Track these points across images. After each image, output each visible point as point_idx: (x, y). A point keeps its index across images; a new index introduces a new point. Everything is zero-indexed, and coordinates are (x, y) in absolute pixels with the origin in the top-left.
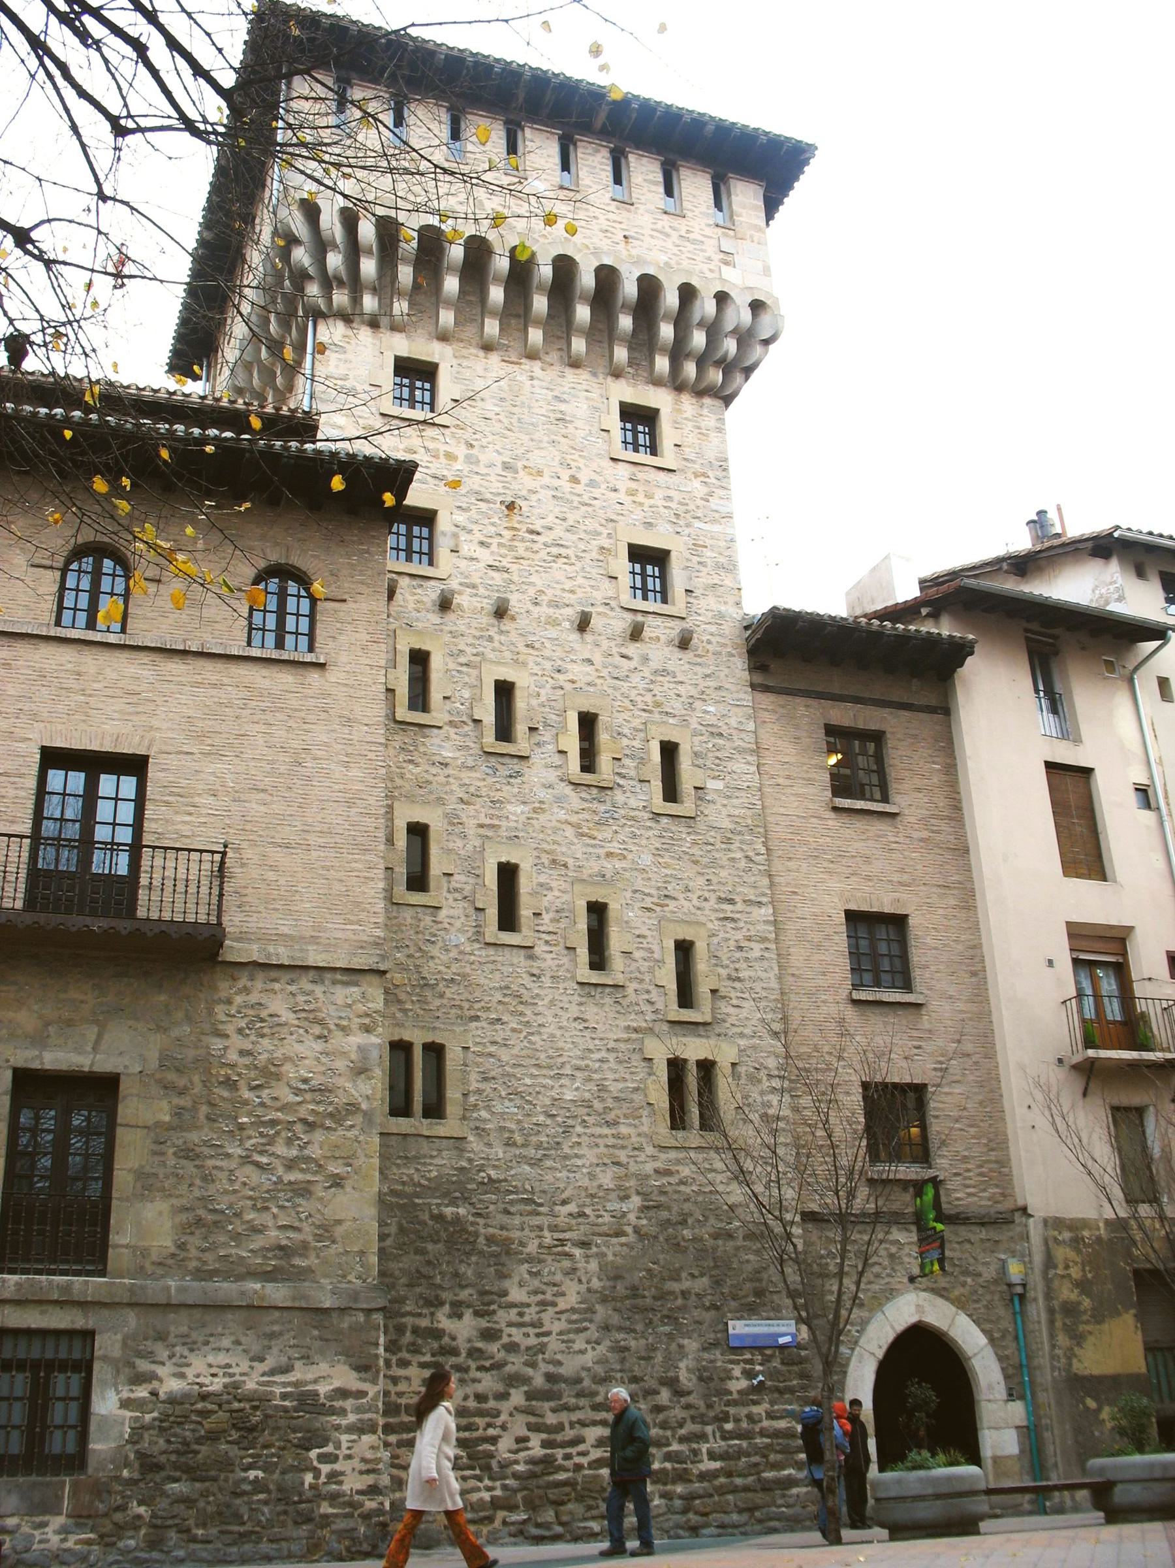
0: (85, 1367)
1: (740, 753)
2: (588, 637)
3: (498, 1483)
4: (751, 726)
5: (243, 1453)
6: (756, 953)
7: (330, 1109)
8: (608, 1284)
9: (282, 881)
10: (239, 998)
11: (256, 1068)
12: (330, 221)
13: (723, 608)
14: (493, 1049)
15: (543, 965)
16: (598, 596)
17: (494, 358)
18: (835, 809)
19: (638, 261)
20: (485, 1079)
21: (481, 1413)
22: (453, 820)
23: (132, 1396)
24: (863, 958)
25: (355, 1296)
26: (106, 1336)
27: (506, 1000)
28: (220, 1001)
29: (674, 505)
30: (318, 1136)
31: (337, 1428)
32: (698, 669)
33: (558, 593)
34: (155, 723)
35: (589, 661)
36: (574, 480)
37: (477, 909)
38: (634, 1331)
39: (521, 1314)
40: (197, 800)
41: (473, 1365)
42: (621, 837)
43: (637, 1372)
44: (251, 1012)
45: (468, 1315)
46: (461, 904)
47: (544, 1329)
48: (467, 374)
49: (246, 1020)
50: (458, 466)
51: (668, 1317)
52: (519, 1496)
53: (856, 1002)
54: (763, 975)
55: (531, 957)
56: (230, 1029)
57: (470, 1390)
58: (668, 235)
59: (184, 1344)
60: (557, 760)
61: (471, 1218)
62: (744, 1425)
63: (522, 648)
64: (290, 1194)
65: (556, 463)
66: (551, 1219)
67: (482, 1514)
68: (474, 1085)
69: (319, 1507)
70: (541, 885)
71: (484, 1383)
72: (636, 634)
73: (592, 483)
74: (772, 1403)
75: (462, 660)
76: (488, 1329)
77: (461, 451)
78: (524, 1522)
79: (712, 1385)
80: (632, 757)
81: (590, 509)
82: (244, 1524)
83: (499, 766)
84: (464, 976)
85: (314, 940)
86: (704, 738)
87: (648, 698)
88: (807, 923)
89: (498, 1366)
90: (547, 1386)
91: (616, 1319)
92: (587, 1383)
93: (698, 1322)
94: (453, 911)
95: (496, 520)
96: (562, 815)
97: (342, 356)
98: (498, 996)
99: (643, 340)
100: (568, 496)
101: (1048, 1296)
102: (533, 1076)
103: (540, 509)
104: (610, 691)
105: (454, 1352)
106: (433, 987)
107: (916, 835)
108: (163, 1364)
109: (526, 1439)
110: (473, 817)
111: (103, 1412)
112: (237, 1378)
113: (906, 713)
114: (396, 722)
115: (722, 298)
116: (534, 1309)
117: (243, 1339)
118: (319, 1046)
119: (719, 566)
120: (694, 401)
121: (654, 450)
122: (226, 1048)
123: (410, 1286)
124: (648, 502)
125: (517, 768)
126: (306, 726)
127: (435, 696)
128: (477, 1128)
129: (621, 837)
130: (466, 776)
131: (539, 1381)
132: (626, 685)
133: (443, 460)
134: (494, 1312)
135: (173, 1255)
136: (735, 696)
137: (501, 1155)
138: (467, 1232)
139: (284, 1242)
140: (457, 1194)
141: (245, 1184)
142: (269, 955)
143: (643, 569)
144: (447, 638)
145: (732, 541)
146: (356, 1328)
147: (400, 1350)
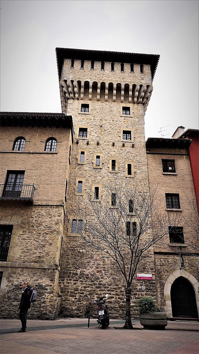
12: (69, 83)
13: (141, 140)
17: (99, 102)
18: (163, 174)
22: (87, 180)
24: (177, 203)
25: (51, 266)
29: (132, 123)
36: (113, 121)
43: (117, 284)
49: (37, 215)
56: (34, 217)
57: (83, 286)
58: (131, 77)
60: (107, 169)
61: (85, 252)
70: (103, 191)
72: (123, 146)
73: (117, 121)
77: (92, 118)
91: (113, 272)
92: (107, 285)
99: (126, 95)
103: (107, 126)
107: (181, 178)
118: (50, 219)
125: (100, 170)
133: (89, 120)
141: (33, 244)
143: (126, 135)
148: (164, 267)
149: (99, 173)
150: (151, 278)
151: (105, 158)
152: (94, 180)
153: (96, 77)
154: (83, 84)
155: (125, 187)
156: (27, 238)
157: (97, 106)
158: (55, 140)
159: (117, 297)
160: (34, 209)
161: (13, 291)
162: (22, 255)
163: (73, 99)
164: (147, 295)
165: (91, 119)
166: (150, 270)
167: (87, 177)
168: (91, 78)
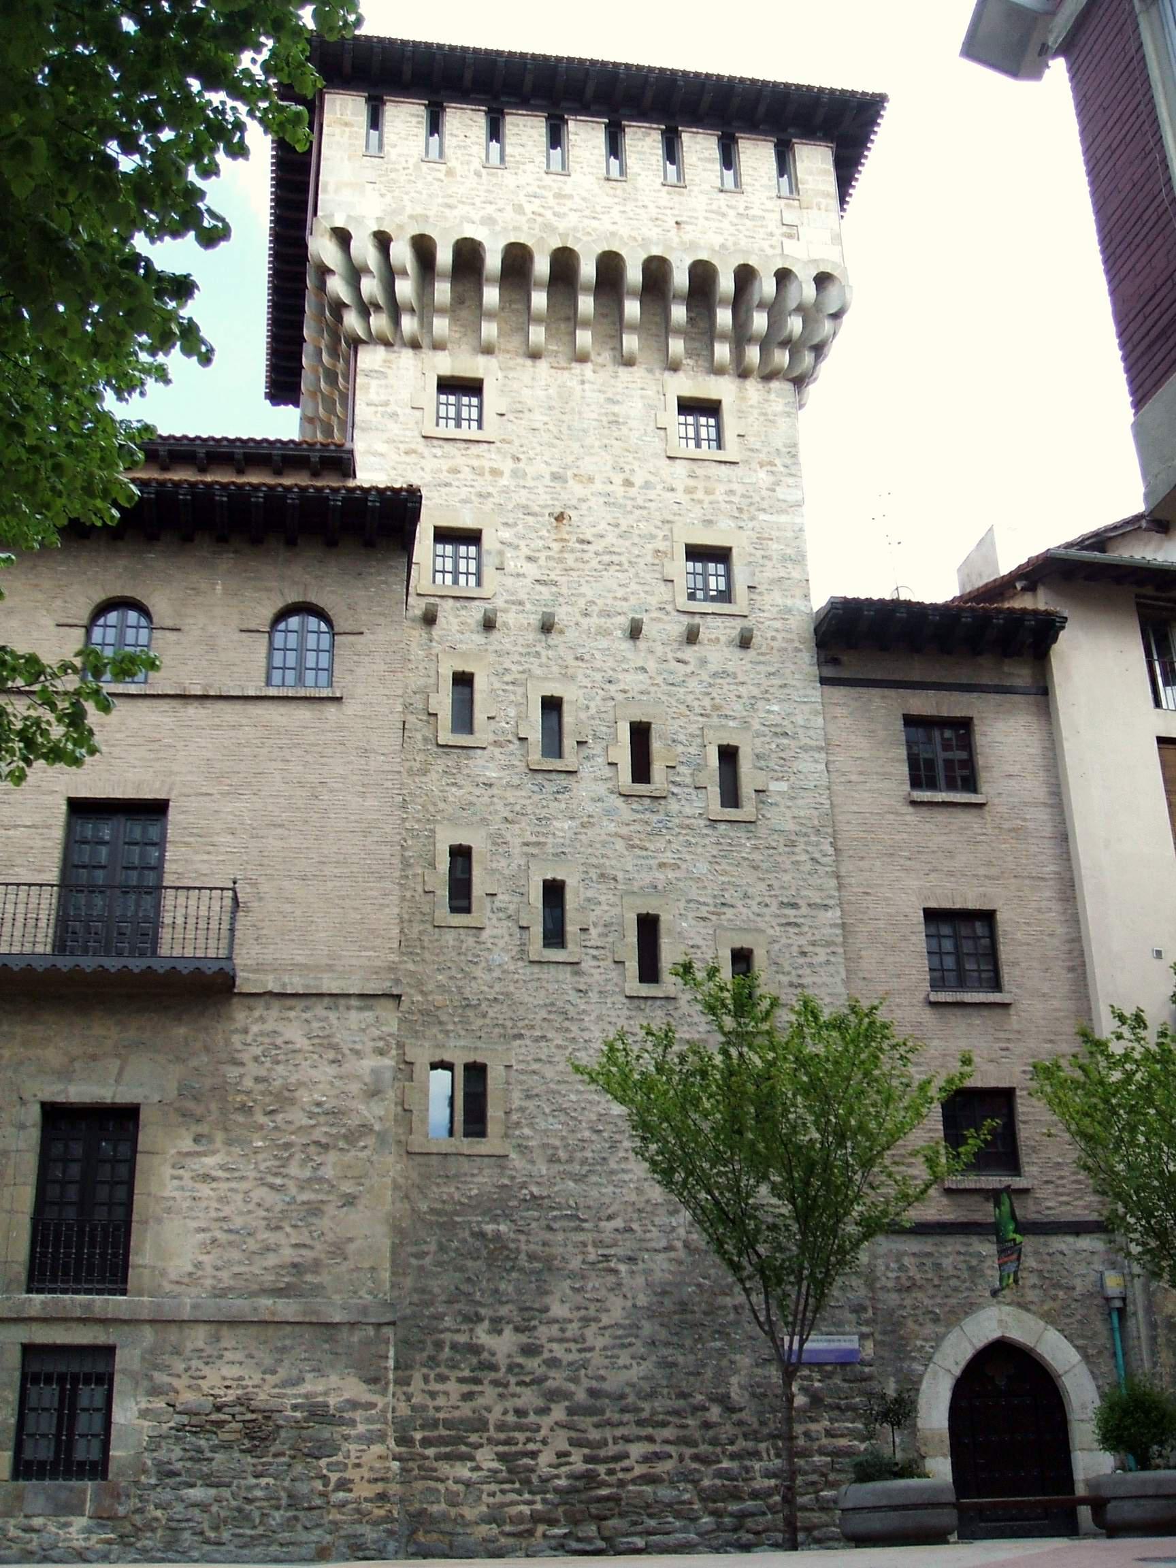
0: (106, 1379)
1: (806, 751)
2: (642, 644)
3: (538, 1498)
4: (820, 721)
6: (822, 958)
7: (343, 1131)
8: (655, 1299)
9: (298, 912)
10: (249, 1030)
12: (364, 250)
13: (789, 602)
14: (536, 1066)
15: (589, 980)
16: (653, 601)
18: (914, 803)
19: (693, 246)
20: (528, 1097)
21: (520, 1428)
22: (498, 841)
25: (365, 1310)
26: (126, 1351)
27: (552, 1017)
28: (236, 1031)
29: (736, 499)
30: (332, 1156)
31: (346, 1438)
32: (760, 668)
33: (609, 601)
34: (176, 768)
35: (643, 670)
36: (628, 483)
37: (521, 928)
38: (682, 1346)
39: (563, 1330)
40: (216, 839)
41: (513, 1380)
42: (675, 846)
44: (267, 1040)
45: (508, 1332)
46: (506, 923)
47: (587, 1344)
48: (515, 385)
50: (504, 481)
52: (561, 1509)
53: (934, 1005)
54: (829, 980)
55: (578, 973)
56: (246, 1057)
57: (509, 1404)
58: (724, 215)
60: (607, 772)
61: (512, 1235)
63: (571, 661)
64: (303, 1214)
65: (609, 467)
66: (595, 1235)
67: (522, 1527)
70: (589, 900)
71: (524, 1398)
72: (692, 637)
73: (647, 485)
74: (831, 1420)
75: (508, 678)
76: (529, 1345)
77: (507, 466)
78: (565, 1536)
79: (766, 1401)
80: (688, 764)
81: (645, 512)
83: (545, 783)
84: (508, 995)
85: (330, 968)
86: (767, 739)
87: (707, 702)
88: (881, 924)
90: (591, 1402)
91: (663, 1334)
92: (631, 1399)
93: (751, 1338)
94: (497, 931)
95: (544, 533)
96: (612, 828)
97: (383, 382)
98: (543, 1013)
101: (1150, 1309)
102: (578, 1092)
103: (593, 518)
104: (664, 698)
105: (493, 1367)
106: (476, 1007)
108: (179, 1376)
109: (567, 1454)
110: (515, 836)
111: (122, 1421)
112: (250, 1389)
113: (997, 697)
114: (439, 746)
115: (783, 276)
116: (575, 1325)
117: (255, 1353)
118: (332, 1070)
119: (785, 559)
120: (760, 386)
122: (241, 1076)
123: (449, 1302)
124: (707, 499)
125: (564, 783)
126: (323, 760)
127: (479, 716)
129: (675, 846)
130: (510, 795)
131: (581, 1396)
132: (682, 690)
133: (488, 477)
134: (535, 1327)
135: (190, 1274)
136: (801, 692)
137: (544, 1172)
138: (507, 1248)
139: (297, 1260)
142: (284, 985)
144: (492, 658)
145: (801, 530)
146: (366, 1343)
147: (438, 1365)
148: (920, 1295)
150: (852, 1352)
151: (593, 711)
152: (534, 839)
153: (519, 209)
154: (444, 257)
155: (710, 896)
156: (220, 1174)
158: (321, 614)
163: (387, 344)
164: (833, 1436)
165: (501, 474)
166: (852, 1317)
168: (489, 221)
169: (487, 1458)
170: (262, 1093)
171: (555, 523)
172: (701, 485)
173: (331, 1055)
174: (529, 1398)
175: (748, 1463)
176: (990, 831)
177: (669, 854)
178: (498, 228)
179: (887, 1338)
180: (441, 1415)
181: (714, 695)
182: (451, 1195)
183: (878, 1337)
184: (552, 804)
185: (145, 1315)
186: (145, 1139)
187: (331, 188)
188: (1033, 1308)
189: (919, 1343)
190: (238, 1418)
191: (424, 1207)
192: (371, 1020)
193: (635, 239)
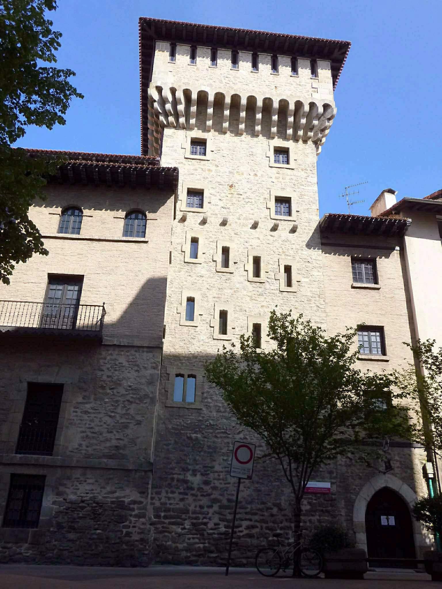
0: (41, 489)
5: (95, 523)
7: (138, 396)
10: (107, 359)
11: (112, 382)
12: (167, 94)
13: (311, 217)
16: (263, 215)
22: (204, 296)
23: (57, 500)
28: (102, 358)
29: (293, 181)
30: (133, 406)
31: (131, 515)
32: (300, 239)
35: (259, 238)
39: (219, 476)
40: (100, 289)
42: (268, 300)
44: (113, 362)
45: (198, 475)
47: (228, 481)
51: (277, 479)
56: (104, 368)
59: (77, 481)
61: (202, 439)
62: (308, 524)
65: (249, 170)
68: (206, 390)
69: (122, 545)
74: (320, 516)
75: (211, 240)
76: (206, 481)
77: (213, 168)
82: (92, 550)
87: (280, 250)
89: (209, 495)
92: (244, 503)
95: (225, 191)
96: (245, 293)
99: (282, 125)
100: (253, 181)
104: (265, 248)
105: (192, 489)
108: (68, 488)
109: (219, 524)
112: (96, 495)
114: (185, 262)
118: (136, 374)
121: (288, 162)
122: (102, 375)
123: (177, 463)
124: (283, 181)
125: (229, 277)
126: (140, 263)
128: (207, 405)
130: (209, 280)
131: (225, 502)
133: (207, 172)
134: (208, 474)
135: (77, 449)
137: (215, 416)
138: (201, 444)
139: (118, 445)
140: (197, 430)
144: (205, 233)
147: (172, 487)
149: (227, 281)
150: (329, 489)
152: (217, 296)
153: (221, 82)
154: (194, 96)
157: (222, 144)
159: (264, 525)
160: (104, 353)
161: (67, 513)
162: (84, 443)
163: (175, 128)
165: (212, 171)
166: (327, 475)
167: (204, 290)
168: (211, 85)
169: (187, 525)
170: (109, 381)
171: (229, 188)
172: (281, 176)
173: (136, 368)
174: (205, 501)
175: (287, 531)
176: (382, 298)
177: (265, 302)
178: (213, 88)
179: (341, 484)
180: (172, 507)
181: (283, 248)
182: (180, 423)
183: (338, 484)
184: (224, 284)
185: (59, 464)
186: (64, 397)
187: (157, 73)
188: (398, 475)
189: (354, 487)
190: (90, 505)
191: (170, 426)
192: (151, 356)
193: (260, 92)
